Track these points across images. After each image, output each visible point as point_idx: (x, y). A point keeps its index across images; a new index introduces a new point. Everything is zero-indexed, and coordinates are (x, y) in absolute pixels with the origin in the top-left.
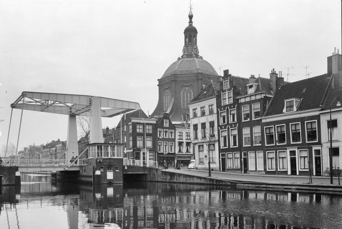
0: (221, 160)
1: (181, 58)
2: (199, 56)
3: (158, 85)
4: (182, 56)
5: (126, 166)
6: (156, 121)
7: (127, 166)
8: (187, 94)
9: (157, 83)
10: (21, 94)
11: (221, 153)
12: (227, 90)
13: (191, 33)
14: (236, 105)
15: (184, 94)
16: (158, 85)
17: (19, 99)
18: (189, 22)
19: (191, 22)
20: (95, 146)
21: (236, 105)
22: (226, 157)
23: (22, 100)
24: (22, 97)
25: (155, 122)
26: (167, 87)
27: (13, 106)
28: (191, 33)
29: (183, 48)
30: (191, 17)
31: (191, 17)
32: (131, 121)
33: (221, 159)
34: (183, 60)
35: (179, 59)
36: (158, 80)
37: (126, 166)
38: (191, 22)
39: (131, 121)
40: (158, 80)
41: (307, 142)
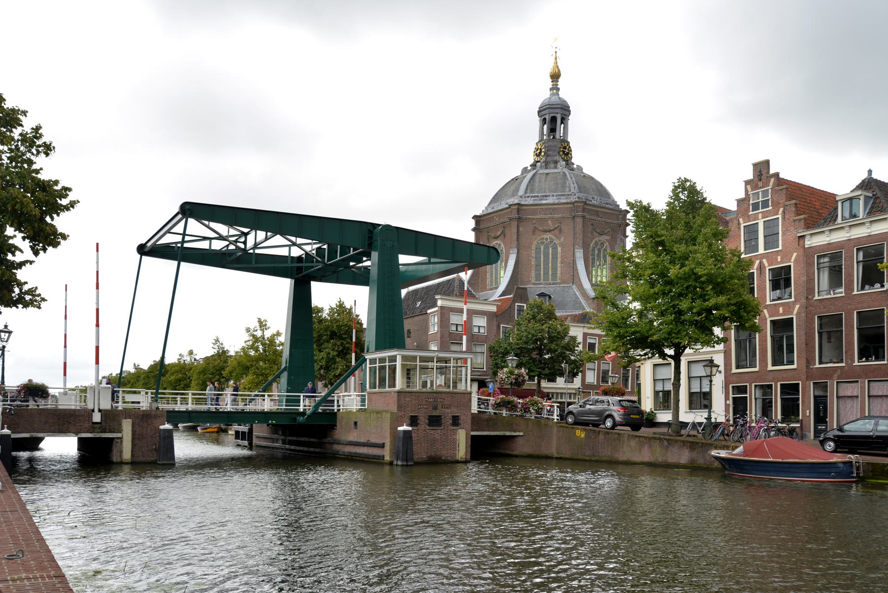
0: (730, 402)
1: (529, 168)
2: (573, 164)
3: (474, 230)
4: (534, 166)
5: (96, 410)
6: (498, 306)
7: (100, 411)
8: (546, 248)
9: (473, 224)
10: (177, 210)
11: (731, 386)
12: (760, 215)
13: (554, 116)
14: (795, 254)
15: (538, 249)
16: (474, 230)
17: (167, 228)
18: (551, 89)
19: (555, 88)
20: (568, 344)
21: (795, 254)
22: (751, 395)
23: (179, 228)
24: (180, 216)
25: (494, 309)
26: (499, 233)
27: (143, 250)
28: (554, 116)
29: (535, 146)
30: (555, 77)
31: (555, 77)
32: (435, 305)
33: (731, 399)
34: (534, 175)
35: (525, 170)
36: (475, 217)
37: (96, 410)
38: (555, 88)
39: (435, 305)
40: (475, 217)
41: (770, 367)
